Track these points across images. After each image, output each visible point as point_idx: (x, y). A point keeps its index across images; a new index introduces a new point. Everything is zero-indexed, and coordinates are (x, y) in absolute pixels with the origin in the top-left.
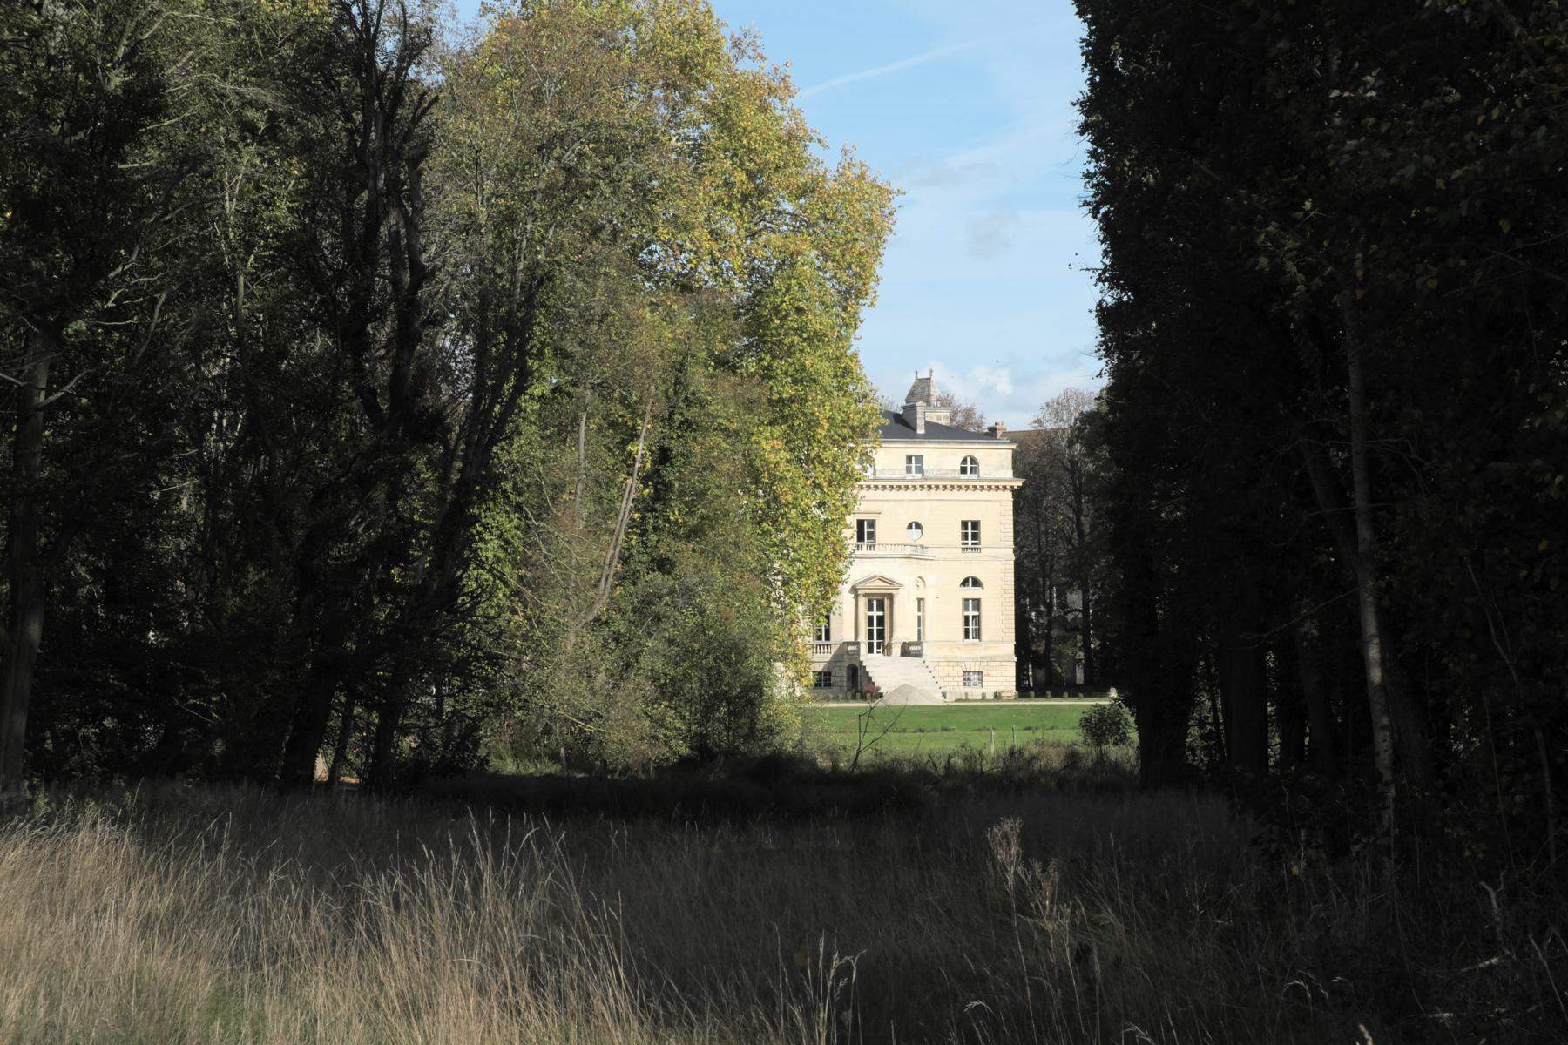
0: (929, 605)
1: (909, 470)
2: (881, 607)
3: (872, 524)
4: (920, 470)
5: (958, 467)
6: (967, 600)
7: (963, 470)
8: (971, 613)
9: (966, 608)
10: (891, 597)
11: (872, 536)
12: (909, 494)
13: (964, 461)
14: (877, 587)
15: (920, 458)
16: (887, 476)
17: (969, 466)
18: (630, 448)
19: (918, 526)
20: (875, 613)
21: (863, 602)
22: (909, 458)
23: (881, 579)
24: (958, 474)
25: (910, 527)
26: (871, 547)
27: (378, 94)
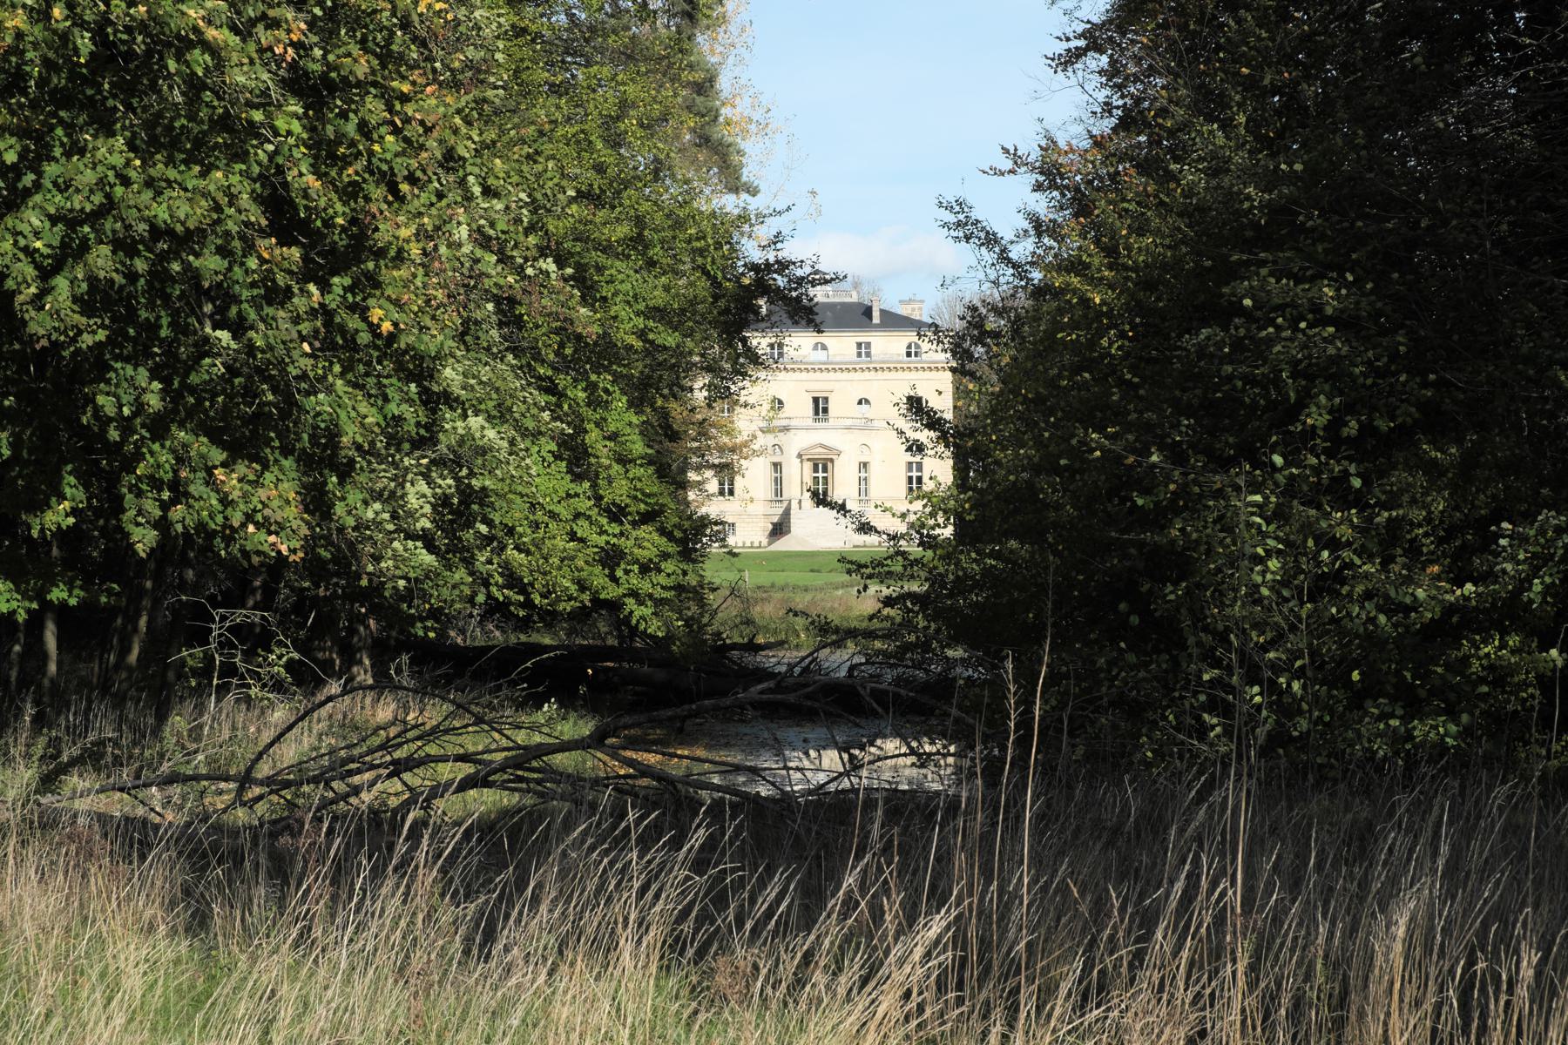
0: (872, 468)
1: (859, 355)
2: (825, 470)
3: (826, 400)
4: (868, 355)
5: (904, 351)
6: (910, 464)
7: (909, 354)
8: (915, 474)
9: (910, 469)
10: (832, 461)
11: (825, 410)
12: (859, 375)
13: (909, 346)
14: (819, 453)
15: (868, 345)
16: (838, 359)
17: (863, 349)
18: (206, 285)
19: (867, 402)
20: (820, 475)
21: (808, 466)
22: (859, 345)
23: (821, 446)
24: (855, 358)
25: (860, 402)
26: (826, 420)
27: (1464, 546)
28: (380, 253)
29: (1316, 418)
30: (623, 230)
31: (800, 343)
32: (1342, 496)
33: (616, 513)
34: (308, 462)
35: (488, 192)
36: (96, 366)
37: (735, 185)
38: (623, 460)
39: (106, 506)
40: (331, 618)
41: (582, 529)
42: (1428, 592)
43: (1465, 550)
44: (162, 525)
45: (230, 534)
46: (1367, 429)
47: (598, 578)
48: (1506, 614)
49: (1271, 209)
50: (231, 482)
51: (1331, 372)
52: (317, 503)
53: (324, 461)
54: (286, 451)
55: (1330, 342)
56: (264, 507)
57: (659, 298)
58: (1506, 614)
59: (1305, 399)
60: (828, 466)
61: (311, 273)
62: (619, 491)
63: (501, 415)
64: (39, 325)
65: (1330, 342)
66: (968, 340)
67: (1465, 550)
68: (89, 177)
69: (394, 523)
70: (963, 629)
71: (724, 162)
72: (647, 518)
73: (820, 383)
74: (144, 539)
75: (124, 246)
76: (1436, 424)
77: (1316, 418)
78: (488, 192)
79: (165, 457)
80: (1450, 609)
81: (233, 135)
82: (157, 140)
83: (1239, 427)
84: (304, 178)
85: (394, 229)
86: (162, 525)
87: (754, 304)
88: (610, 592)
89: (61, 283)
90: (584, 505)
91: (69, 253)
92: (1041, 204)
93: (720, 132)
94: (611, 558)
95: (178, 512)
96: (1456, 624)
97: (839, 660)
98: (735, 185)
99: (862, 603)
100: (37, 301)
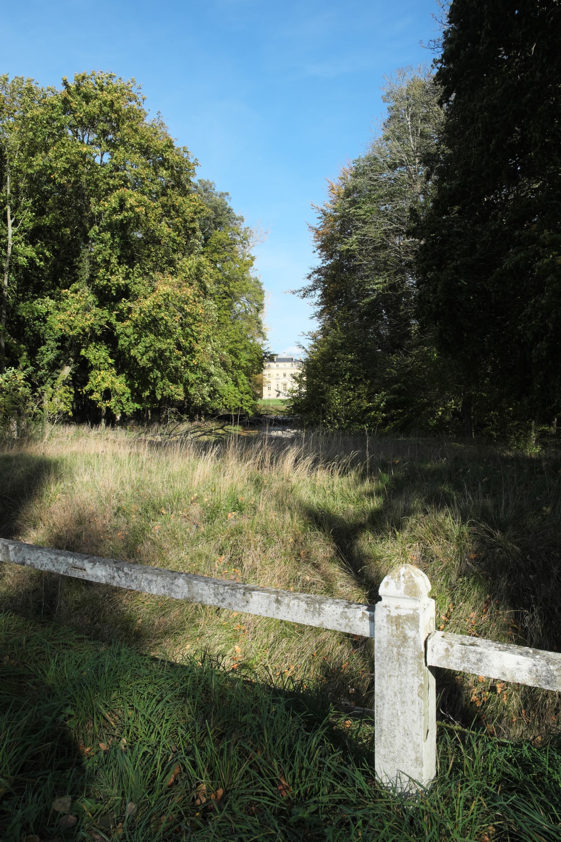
17: (278, 366)
28: (195, 352)
29: (347, 377)
30: (242, 347)
31: (272, 364)
32: (351, 389)
33: (242, 393)
34: (185, 385)
35: (214, 341)
36: (151, 370)
37: (265, 339)
38: (244, 384)
39: (153, 393)
40: (189, 410)
41: (237, 395)
42: (366, 404)
43: (370, 398)
44: (162, 395)
45: (172, 396)
46: (355, 379)
47: (239, 403)
48: (377, 408)
49: (341, 343)
50: (172, 388)
51: (350, 370)
52: (186, 391)
53: (186, 384)
54: (181, 382)
55: (349, 365)
56: (177, 392)
57: (248, 358)
58: (377, 408)
59: (346, 373)
60: (280, 385)
61: (184, 355)
62: (242, 389)
63: (220, 376)
64: (141, 363)
65: (349, 365)
66: (307, 363)
67: (370, 398)
68: (149, 341)
69: (200, 394)
70: (299, 411)
71: (262, 334)
72: (247, 393)
73: (284, 371)
74: (159, 397)
75: (155, 351)
76: (366, 377)
77: (347, 377)
78: (214, 341)
79: (162, 384)
80: (367, 407)
81: (168, 333)
82: (158, 334)
83: (334, 379)
84: (181, 340)
85: (198, 347)
86: (162, 395)
87: (262, 360)
88: (241, 406)
89: (144, 357)
90: (237, 391)
91: (146, 352)
92: (312, 342)
93: (263, 330)
94: (241, 400)
95: (164, 393)
96: (369, 410)
97: (280, 417)
98: (265, 339)
99: (284, 408)
100: (140, 360)
